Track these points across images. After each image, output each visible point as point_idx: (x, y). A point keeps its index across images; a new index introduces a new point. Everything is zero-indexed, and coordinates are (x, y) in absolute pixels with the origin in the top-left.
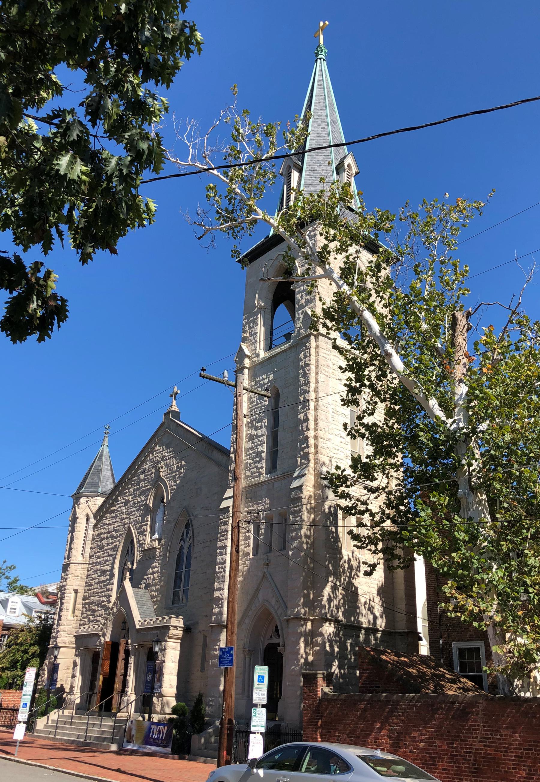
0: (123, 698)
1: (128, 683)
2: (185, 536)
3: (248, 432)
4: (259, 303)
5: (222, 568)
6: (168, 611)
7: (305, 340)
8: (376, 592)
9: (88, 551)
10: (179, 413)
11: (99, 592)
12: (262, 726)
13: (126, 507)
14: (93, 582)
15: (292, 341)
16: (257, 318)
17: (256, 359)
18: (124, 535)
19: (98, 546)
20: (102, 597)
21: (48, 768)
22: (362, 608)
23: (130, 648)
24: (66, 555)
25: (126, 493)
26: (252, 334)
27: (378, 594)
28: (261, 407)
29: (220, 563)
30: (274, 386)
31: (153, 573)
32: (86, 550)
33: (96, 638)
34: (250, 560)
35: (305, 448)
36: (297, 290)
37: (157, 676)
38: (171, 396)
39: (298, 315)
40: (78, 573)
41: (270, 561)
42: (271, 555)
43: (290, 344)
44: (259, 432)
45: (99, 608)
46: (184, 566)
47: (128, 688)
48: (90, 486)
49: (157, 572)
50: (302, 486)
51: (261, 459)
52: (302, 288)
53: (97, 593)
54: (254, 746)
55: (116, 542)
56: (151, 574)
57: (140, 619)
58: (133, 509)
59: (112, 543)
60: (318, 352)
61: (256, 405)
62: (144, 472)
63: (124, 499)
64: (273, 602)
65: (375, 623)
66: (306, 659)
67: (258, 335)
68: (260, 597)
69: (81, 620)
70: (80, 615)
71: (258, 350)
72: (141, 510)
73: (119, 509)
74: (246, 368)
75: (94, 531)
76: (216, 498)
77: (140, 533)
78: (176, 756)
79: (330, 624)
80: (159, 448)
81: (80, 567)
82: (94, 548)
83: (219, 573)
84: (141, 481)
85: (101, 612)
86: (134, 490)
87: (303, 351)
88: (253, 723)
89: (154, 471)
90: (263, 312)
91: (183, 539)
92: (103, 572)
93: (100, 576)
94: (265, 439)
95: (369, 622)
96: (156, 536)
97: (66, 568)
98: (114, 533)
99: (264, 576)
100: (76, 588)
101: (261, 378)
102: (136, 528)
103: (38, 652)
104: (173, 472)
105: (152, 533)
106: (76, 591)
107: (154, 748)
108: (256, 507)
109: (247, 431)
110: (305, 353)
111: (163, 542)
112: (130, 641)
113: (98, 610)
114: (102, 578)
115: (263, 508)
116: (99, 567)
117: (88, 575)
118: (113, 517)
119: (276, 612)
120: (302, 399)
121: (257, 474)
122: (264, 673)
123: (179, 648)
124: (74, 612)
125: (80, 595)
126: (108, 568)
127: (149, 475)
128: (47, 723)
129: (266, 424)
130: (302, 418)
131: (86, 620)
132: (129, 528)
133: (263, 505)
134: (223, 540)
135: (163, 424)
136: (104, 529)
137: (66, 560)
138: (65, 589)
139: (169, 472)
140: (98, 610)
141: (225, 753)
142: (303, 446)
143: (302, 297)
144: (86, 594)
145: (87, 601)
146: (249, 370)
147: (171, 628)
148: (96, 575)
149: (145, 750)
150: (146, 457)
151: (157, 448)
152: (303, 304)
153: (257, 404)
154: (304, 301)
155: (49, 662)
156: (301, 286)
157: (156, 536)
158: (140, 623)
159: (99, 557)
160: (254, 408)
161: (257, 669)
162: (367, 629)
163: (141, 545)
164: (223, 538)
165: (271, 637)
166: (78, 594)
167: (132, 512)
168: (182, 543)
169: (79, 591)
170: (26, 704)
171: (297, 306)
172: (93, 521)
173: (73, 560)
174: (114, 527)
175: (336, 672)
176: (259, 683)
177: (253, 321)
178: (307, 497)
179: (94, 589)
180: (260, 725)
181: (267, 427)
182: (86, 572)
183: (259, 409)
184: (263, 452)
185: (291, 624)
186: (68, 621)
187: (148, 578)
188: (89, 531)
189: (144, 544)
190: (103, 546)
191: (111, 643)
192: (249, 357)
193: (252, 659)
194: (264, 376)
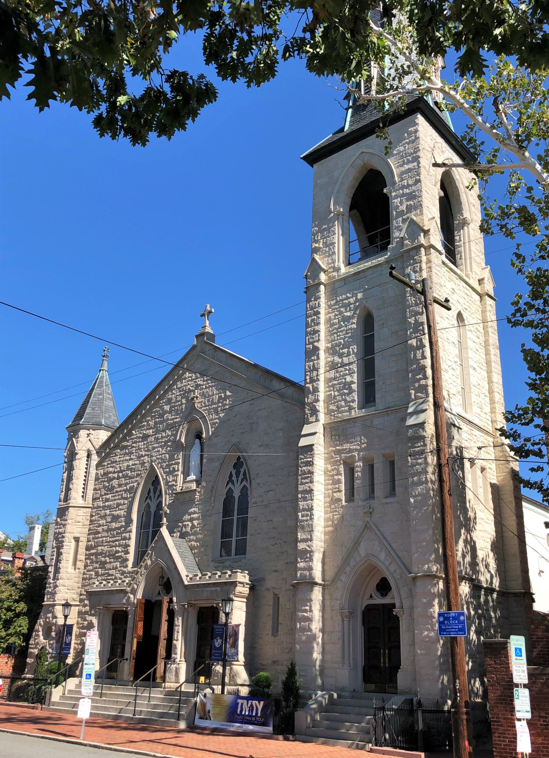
0: (169, 666)
1: (176, 648)
2: (234, 478)
3: (329, 359)
4: (335, 208)
5: (307, 515)
6: (217, 564)
7: (411, 253)
8: (490, 548)
10: (213, 336)
11: (110, 541)
12: (527, 712)
13: (145, 442)
14: (100, 529)
15: (389, 254)
16: (333, 226)
17: (335, 274)
18: (144, 475)
19: (104, 487)
20: (115, 546)
22: (481, 565)
23: (176, 607)
24: (62, 497)
25: (144, 426)
26: (326, 245)
27: (492, 550)
28: (347, 330)
29: (304, 510)
30: (365, 306)
31: (191, 520)
33: (122, 595)
34: (342, 507)
35: (420, 379)
36: (393, 194)
37: (230, 641)
38: (203, 315)
39: (397, 223)
41: (373, 509)
42: (375, 503)
43: (386, 257)
44: (346, 360)
45: (112, 560)
46: (236, 512)
47: (176, 654)
48: (91, 416)
49: (198, 519)
50: (424, 423)
51: (351, 391)
52: (401, 191)
53: (107, 542)
54: (521, 736)
55: (132, 482)
56: (189, 521)
57: (187, 574)
58: (155, 445)
59: (126, 484)
60: (430, 268)
61: (338, 328)
62: (169, 402)
63: (140, 433)
64: (382, 556)
65: (491, 583)
67: (336, 245)
68: (362, 550)
69: (84, 574)
70: (83, 567)
71: (337, 264)
72: (168, 446)
73: (135, 445)
74: (323, 284)
75: (97, 470)
76: (281, 434)
77: (168, 474)
78: (281, 737)
79: (465, 583)
80: (190, 375)
81: (82, 512)
82: (100, 489)
83: (303, 521)
84: (166, 412)
85: (114, 564)
86: (156, 423)
87: (410, 265)
88: (517, 708)
89: (184, 401)
90: (340, 219)
91: (230, 480)
92: (115, 518)
93: (110, 522)
94: (354, 367)
95: (487, 581)
96: (192, 477)
97: (62, 512)
98: (129, 472)
99: (366, 527)
100: (77, 535)
101: (344, 296)
102: (161, 467)
103: (25, 610)
104: (213, 403)
105: (186, 474)
106: (77, 540)
107: (251, 727)
108: (347, 446)
109: (326, 358)
110: (414, 268)
111: (204, 484)
112: (175, 599)
113: (110, 563)
114: (114, 525)
115: (359, 448)
116: (108, 512)
117: (91, 521)
118: (126, 453)
119: (388, 568)
120: (413, 322)
121: (347, 408)
123: (245, 609)
124: (75, 564)
125: (83, 545)
126: (122, 513)
127: (177, 406)
128: (64, 694)
129: (355, 350)
130: (415, 345)
131: (93, 573)
132: (152, 467)
133: (358, 445)
134: (307, 483)
135: (194, 347)
136: (112, 467)
137: (62, 503)
138: (63, 537)
139: (207, 404)
140: (110, 563)
141: (467, 743)
142: (418, 377)
143: (401, 203)
144: (90, 543)
145: (93, 551)
146: (325, 287)
147: (238, 585)
148: (104, 521)
149: (232, 729)
150: (171, 386)
151: (187, 375)
152: (403, 210)
153: (341, 326)
154: (405, 207)
155: (45, 622)
156: (398, 190)
157: (192, 477)
158: (188, 578)
159: (107, 500)
160: (335, 331)
161: (513, 639)
162: (486, 589)
163: (171, 487)
164: (307, 481)
165: (371, 596)
166: (80, 543)
167: (154, 448)
168: (230, 485)
169: (81, 539)
170: (90, 675)
171: (395, 213)
172: (95, 459)
173: (72, 502)
174: (128, 466)
175: (474, 639)
177: (328, 230)
178: (430, 436)
179: (102, 537)
180: (524, 709)
181: (356, 354)
182: (89, 518)
183: (344, 332)
184: (352, 382)
185: (419, 583)
186: (68, 575)
187: (185, 526)
188: (91, 469)
189: (176, 486)
190: (113, 488)
191: (144, 601)
192: (325, 271)
193: (351, 623)
194: (348, 295)
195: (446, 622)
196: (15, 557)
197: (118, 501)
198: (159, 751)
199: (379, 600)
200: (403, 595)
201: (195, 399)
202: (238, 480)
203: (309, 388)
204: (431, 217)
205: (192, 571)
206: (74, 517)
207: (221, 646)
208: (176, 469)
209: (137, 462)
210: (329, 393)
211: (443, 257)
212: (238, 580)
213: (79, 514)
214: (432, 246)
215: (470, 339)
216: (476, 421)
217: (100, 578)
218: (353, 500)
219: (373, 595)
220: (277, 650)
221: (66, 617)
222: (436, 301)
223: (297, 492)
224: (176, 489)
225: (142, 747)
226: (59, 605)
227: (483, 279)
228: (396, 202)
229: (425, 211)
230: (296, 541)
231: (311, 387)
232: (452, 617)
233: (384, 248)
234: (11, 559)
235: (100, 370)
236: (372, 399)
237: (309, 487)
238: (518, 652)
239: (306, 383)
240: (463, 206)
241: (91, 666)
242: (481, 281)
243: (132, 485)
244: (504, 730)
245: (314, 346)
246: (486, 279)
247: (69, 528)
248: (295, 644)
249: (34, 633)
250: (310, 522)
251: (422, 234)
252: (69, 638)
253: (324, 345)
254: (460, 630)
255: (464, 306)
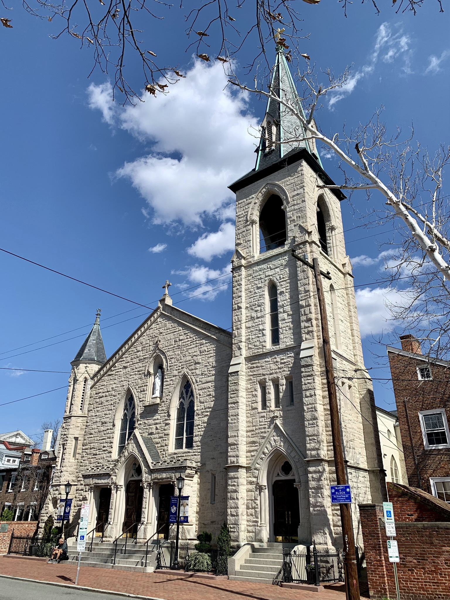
2: (185, 395)
9: (86, 407)
21: (129, 596)
32: (85, 406)
40: (79, 425)
66: (303, 372)
67: (251, 242)
71: (252, 253)
74: (243, 266)
81: (80, 420)
83: (231, 423)
106: (76, 439)
122: (390, 509)
130: (304, 305)
131: (87, 462)
139: (166, 344)
161: (385, 505)
165: (278, 475)
169: (79, 439)
176: (389, 518)
183: (258, 297)
195: (336, 493)
196: (34, 452)
197: (105, 412)
198: (132, 592)
199: (283, 477)
200: (301, 473)
201: (159, 342)
202: (187, 397)
203: (235, 333)
204: (312, 224)
205: (156, 459)
206: (74, 423)
207: (176, 512)
208: (145, 390)
209: (119, 385)
210: (248, 337)
211: (320, 249)
212: (187, 465)
213: (78, 422)
214: (314, 242)
215: (338, 301)
216: (345, 355)
217: (92, 465)
218: (293, 405)
219: (280, 474)
220: (214, 514)
221: (67, 494)
222: (322, 273)
223: (227, 403)
224: (145, 403)
225: (120, 589)
226: (63, 485)
227: (345, 264)
228: (289, 214)
229: (308, 220)
230: (227, 437)
231: (236, 333)
232: (341, 489)
233: (282, 244)
234: (31, 453)
235: (94, 324)
236: (276, 341)
237: (236, 400)
238: (389, 512)
239: (233, 330)
240: (331, 218)
241: (85, 530)
242: (344, 265)
243: (115, 401)
244: (375, 568)
245: (238, 306)
246: (347, 264)
247: (71, 431)
248: (227, 508)
249: (45, 505)
250: (237, 424)
251: (307, 235)
252: (69, 508)
253: (244, 305)
254: (347, 498)
255: (334, 281)
